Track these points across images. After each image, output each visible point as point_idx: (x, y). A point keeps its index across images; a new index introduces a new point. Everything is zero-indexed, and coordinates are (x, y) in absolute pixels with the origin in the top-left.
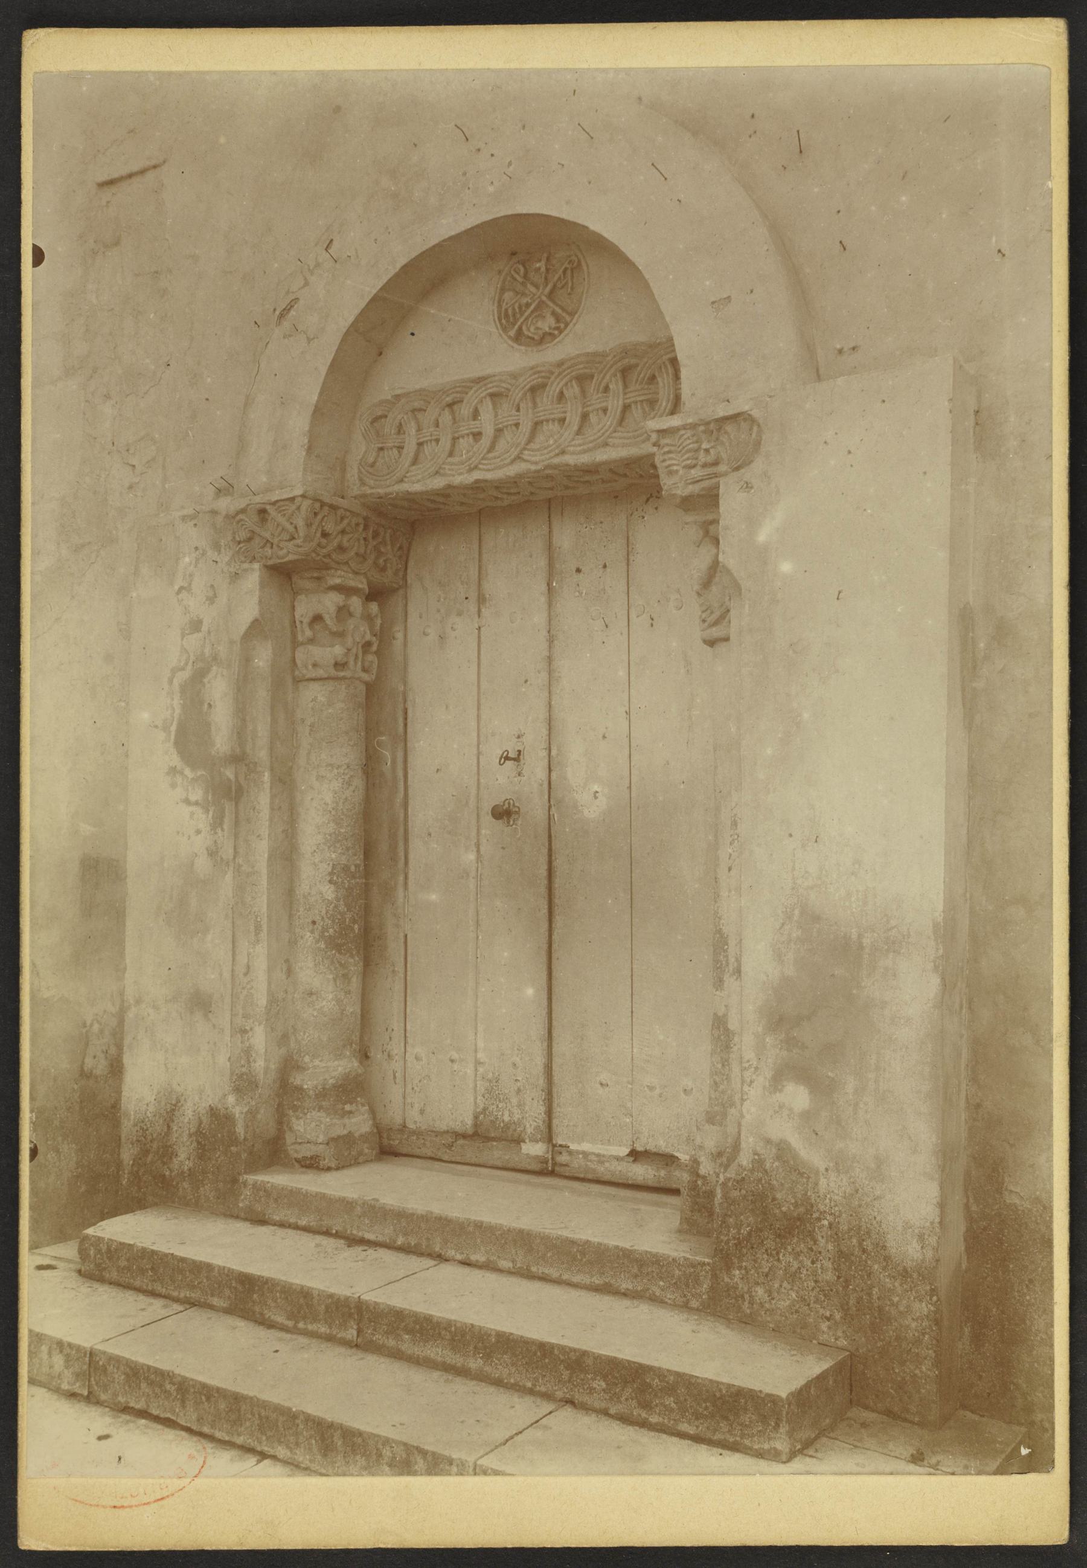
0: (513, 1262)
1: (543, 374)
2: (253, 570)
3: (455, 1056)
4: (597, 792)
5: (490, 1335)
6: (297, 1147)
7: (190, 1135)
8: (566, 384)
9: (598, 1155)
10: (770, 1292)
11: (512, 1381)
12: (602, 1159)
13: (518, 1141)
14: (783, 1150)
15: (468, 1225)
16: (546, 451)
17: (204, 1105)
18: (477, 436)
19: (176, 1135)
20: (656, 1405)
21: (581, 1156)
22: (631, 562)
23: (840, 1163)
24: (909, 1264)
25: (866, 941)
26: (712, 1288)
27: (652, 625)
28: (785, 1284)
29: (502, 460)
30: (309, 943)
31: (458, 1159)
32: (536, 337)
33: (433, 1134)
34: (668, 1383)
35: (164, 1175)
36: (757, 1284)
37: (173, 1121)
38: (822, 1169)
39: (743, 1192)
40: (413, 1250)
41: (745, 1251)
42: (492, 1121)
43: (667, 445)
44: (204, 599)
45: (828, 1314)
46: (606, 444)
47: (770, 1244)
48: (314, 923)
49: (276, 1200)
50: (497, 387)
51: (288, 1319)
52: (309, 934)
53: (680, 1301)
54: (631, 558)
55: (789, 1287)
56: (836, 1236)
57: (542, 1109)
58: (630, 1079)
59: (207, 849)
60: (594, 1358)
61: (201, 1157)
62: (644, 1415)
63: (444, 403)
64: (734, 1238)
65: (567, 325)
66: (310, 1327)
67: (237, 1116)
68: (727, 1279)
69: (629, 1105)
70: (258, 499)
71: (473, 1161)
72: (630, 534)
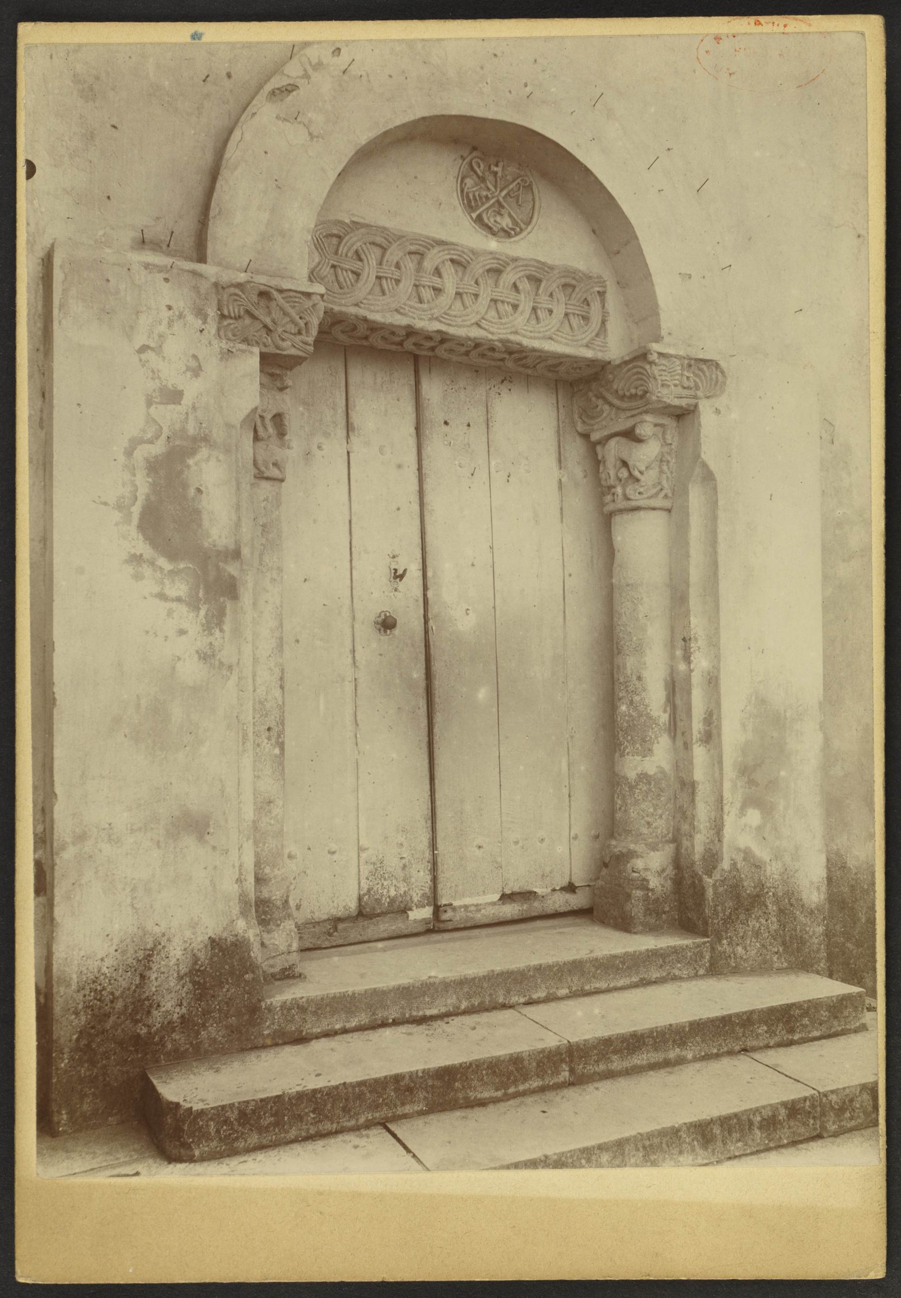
0: (569, 988)
1: (501, 262)
2: (252, 353)
3: (334, 847)
4: (468, 609)
5: (684, 1027)
6: (271, 962)
7: (180, 978)
8: (519, 278)
9: (477, 905)
10: (745, 948)
11: (703, 1054)
12: (480, 907)
13: (404, 911)
14: (747, 854)
15: (529, 971)
16: (502, 327)
17: (199, 939)
18: (438, 291)
19: (155, 984)
20: (798, 1027)
21: (462, 910)
22: (490, 427)
23: (777, 856)
24: (813, 906)
25: (788, 714)
26: (711, 957)
27: (508, 481)
28: (754, 940)
29: (463, 321)
30: (267, 750)
31: (340, 942)
32: (495, 229)
33: (311, 926)
34: (803, 1009)
35: (139, 1035)
36: (738, 945)
37: (150, 969)
38: (768, 861)
39: (725, 887)
40: (478, 1009)
41: (728, 926)
42: (376, 900)
43: (664, 365)
44: (184, 368)
45: (776, 950)
46: (551, 338)
47: (742, 917)
48: (269, 729)
49: (315, 1013)
50: (459, 255)
51: (497, 1090)
52: (266, 741)
53: (692, 973)
54: (491, 424)
55: (755, 941)
56: (777, 902)
57: (429, 878)
58: (500, 839)
59: (197, 652)
60: (759, 1012)
61: (199, 998)
62: (790, 1037)
63: (408, 250)
64: (722, 919)
65: (522, 230)
66: (521, 1088)
67: (252, 939)
68: (720, 949)
69: (499, 859)
70: (262, 279)
71: (356, 940)
72: (489, 405)
